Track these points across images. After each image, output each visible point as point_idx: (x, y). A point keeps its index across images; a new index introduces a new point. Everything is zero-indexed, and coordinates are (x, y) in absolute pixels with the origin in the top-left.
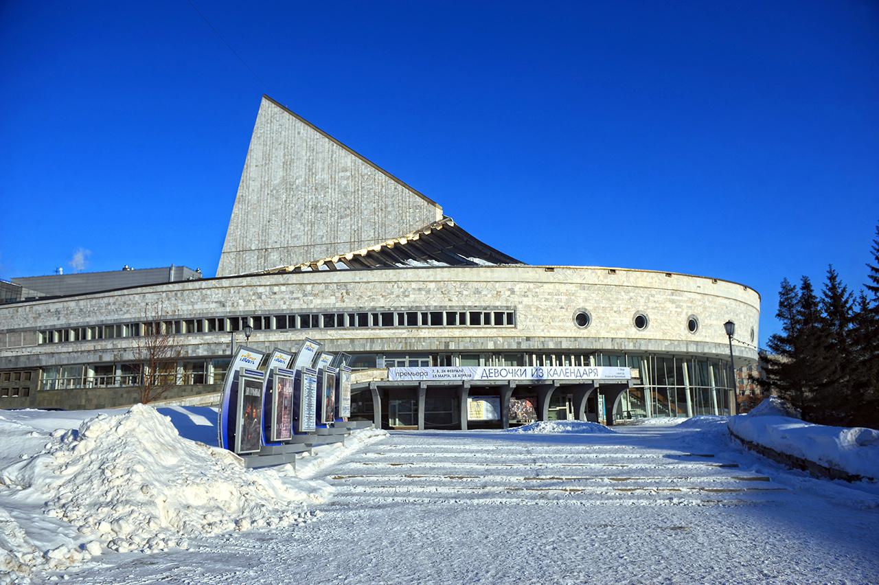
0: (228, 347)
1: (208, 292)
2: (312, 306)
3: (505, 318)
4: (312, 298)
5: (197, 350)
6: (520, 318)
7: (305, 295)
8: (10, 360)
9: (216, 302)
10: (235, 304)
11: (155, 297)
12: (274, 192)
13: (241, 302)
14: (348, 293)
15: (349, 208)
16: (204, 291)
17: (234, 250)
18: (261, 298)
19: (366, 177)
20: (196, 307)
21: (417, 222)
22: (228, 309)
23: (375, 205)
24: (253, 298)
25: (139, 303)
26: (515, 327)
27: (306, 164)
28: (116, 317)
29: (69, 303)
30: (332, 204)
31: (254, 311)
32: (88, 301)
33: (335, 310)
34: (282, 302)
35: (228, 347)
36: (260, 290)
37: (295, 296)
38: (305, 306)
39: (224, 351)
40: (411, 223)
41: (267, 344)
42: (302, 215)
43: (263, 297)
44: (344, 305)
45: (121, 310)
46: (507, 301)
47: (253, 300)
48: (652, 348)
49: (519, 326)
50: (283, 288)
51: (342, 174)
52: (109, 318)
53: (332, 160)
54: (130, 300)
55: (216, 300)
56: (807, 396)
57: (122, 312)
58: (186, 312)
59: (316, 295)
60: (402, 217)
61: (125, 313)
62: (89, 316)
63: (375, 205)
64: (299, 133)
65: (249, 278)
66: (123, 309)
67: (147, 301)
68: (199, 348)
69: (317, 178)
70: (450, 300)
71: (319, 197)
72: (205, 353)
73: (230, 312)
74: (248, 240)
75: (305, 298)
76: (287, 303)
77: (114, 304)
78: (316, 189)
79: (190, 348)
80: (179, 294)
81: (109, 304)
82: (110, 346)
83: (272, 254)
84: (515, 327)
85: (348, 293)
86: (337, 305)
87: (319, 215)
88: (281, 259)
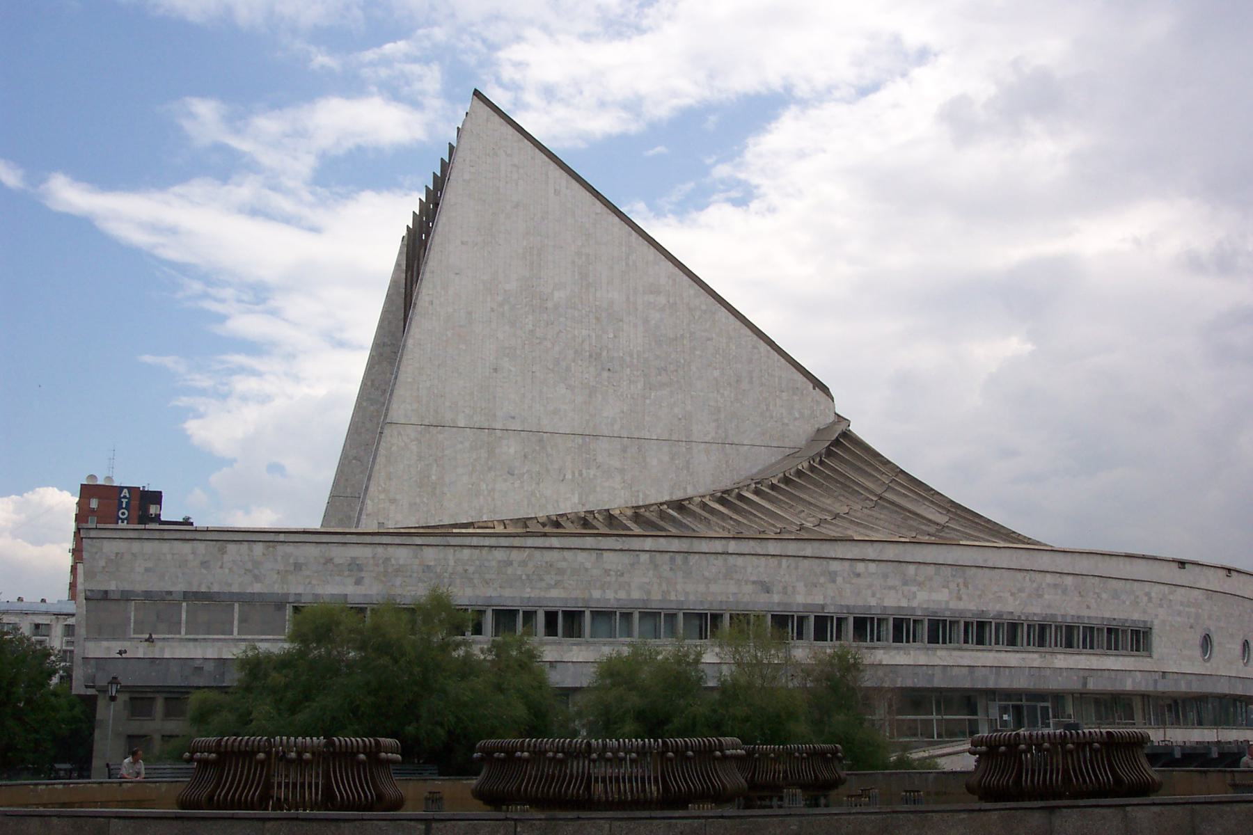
1: (740, 561)
2: (915, 604)
3: (1137, 638)
4: (914, 589)
6: (1159, 643)
7: (905, 583)
8: (201, 669)
9: (754, 582)
10: (790, 590)
11: (626, 559)
12: (506, 308)
13: (800, 586)
14: (966, 586)
15: (665, 370)
16: (731, 559)
17: (414, 420)
18: (834, 581)
19: (698, 313)
20: (714, 588)
21: (796, 419)
22: (776, 598)
24: (822, 580)
25: (586, 570)
26: (1150, 656)
27: (573, 262)
28: (528, 592)
29: (390, 549)
31: (823, 607)
32: (451, 550)
33: (948, 613)
34: (869, 592)
36: (835, 566)
37: (890, 582)
38: (904, 603)
40: (786, 421)
42: (568, 369)
43: (839, 580)
44: (961, 605)
45: (542, 580)
46: (1145, 612)
47: (822, 585)
48: (1004, 683)
49: (1155, 655)
51: (651, 298)
52: (508, 593)
53: (627, 264)
54: (565, 560)
57: (543, 584)
58: (692, 598)
59: (920, 584)
60: (768, 405)
61: (550, 587)
63: (716, 373)
64: (557, 192)
65: (816, 544)
67: (608, 567)
69: (598, 294)
70: (1088, 607)
71: (605, 336)
73: (779, 604)
74: (448, 404)
75: (906, 588)
76: (878, 596)
78: (598, 319)
80: (679, 558)
81: (510, 563)
84: (1150, 656)
85: (966, 586)
86: (952, 605)
87: (605, 374)
88: (525, 456)
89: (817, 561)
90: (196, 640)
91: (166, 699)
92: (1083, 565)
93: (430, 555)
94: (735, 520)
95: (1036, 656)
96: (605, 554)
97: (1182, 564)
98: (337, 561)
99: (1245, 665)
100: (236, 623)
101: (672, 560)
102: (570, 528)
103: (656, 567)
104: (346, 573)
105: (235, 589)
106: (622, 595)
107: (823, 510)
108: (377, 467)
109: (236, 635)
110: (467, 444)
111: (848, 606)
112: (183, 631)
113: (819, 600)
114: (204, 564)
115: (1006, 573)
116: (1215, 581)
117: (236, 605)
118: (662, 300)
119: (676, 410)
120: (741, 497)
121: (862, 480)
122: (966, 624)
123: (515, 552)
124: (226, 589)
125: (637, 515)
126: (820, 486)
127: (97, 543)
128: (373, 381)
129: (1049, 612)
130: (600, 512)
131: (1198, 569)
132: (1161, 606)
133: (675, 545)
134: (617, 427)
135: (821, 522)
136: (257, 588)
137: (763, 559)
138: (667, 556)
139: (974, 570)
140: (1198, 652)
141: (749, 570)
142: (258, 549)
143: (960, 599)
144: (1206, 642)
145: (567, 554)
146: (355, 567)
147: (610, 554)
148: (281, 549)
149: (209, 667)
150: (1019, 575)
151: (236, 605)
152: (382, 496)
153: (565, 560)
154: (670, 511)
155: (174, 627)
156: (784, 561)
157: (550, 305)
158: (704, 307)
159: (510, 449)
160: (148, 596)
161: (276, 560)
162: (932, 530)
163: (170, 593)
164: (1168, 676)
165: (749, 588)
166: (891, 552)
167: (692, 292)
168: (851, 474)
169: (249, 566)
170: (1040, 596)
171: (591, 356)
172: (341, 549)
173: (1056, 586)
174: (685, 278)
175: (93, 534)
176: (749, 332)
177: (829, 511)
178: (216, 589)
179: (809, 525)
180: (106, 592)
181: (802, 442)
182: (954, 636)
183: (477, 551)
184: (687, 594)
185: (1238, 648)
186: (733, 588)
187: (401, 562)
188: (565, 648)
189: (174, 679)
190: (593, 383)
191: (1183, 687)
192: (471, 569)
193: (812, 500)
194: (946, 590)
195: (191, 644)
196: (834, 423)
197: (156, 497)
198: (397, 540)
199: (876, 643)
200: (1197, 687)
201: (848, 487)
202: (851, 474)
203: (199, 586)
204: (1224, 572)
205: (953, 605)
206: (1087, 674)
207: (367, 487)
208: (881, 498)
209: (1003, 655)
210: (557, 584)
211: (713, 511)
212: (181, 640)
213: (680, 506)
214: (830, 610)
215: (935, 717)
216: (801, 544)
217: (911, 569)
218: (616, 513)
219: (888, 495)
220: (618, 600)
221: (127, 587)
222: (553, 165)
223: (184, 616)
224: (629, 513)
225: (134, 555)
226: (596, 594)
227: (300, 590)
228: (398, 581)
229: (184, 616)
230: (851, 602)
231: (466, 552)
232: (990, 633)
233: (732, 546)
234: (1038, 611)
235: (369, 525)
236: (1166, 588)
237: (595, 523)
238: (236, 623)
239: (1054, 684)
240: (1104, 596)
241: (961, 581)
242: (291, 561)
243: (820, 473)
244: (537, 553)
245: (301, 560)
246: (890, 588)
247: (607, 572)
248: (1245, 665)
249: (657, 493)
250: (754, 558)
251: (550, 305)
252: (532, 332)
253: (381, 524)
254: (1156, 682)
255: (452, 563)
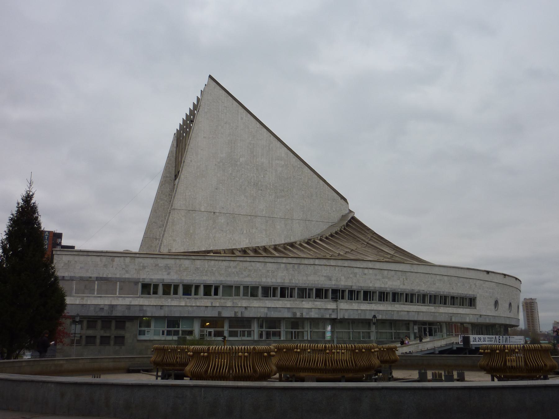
0: (333, 312)
1: (320, 267)
2: (387, 286)
3: (471, 302)
4: (387, 280)
5: (310, 313)
6: (479, 303)
7: (383, 278)
9: (325, 276)
11: (275, 266)
13: (343, 278)
14: (407, 279)
16: (316, 266)
22: (333, 283)
23: (303, 192)
26: (476, 308)
28: (236, 279)
29: (182, 261)
30: (270, 185)
31: (351, 286)
32: (207, 261)
33: (399, 290)
35: (333, 312)
36: (356, 270)
38: (383, 286)
39: (330, 315)
41: (359, 312)
42: (245, 189)
43: (358, 276)
44: (404, 287)
45: (242, 274)
47: (351, 278)
49: (477, 308)
50: (371, 271)
52: (229, 279)
53: (269, 148)
54: (251, 266)
55: (325, 274)
56: (457, 335)
58: (301, 282)
62: (206, 275)
64: (242, 118)
66: (244, 273)
68: (311, 312)
69: (257, 160)
72: (316, 316)
73: (334, 285)
77: (235, 267)
78: (257, 170)
79: (305, 311)
80: (296, 266)
82: (229, 304)
83: (220, 218)
84: (476, 308)
85: (407, 279)
87: (260, 192)
89: (349, 268)
90: (101, 297)
91: (88, 321)
92: (452, 272)
93: (198, 263)
94: (314, 251)
95: (433, 308)
96: (268, 264)
97: (488, 272)
98: (160, 265)
99: (510, 312)
100: (118, 290)
101: (293, 267)
102: (238, 254)
103: (287, 270)
104: (164, 270)
105: (118, 276)
106: (274, 280)
107: (347, 248)
108: (168, 227)
109: (96, 294)
110: (205, 218)
111: (361, 287)
112: (96, 293)
113: (350, 284)
114: (105, 266)
115: (422, 275)
116: (500, 280)
117: (118, 283)
118: (283, 163)
119: (287, 207)
120: (315, 242)
121: (360, 236)
122: (406, 294)
123: (232, 263)
124: (114, 276)
125: (276, 248)
126: (345, 238)
127: (60, 256)
128: (162, 191)
129: (438, 290)
130: (261, 247)
131: (493, 274)
132: (480, 289)
133: (295, 261)
134: (264, 213)
135: (346, 252)
136: (127, 276)
137: (329, 267)
138: (292, 265)
139: (410, 273)
140: (493, 307)
141: (323, 271)
142: (128, 260)
143: (404, 285)
144: (496, 303)
145: (253, 263)
146: (167, 268)
147: (270, 264)
148: (138, 260)
149: (106, 308)
150: (427, 276)
151: (118, 283)
152: (170, 238)
153: (251, 266)
154: (288, 247)
155: (92, 291)
156: (337, 268)
157: (238, 163)
158: (299, 166)
159: (222, 220)
160: (82, 279)
161: (135, 265)
162: (389, 256)
163: (91, 277)
164: (482, 317)
165: (323, 279)
166: (378, 265)
167: (294, 160)
168: (356, 234)
169: (124, 267)
170: (435, 284)
171: (254, 184)
172: (162, 261)
173: (440, 280)
174: (292, 154)
175: (58, 253)
176: (316, 177)
177: (349, 248)
178: (110, 276)
179: (341, 253)
180: (64, 277)
181: (336, 220)
182: (374, 298)
183: (217, 262)
184: (299, 280)
185: (508, 305)
186: (305, 278)
187: (187, 266)
188: (251, 301)
189: (91, 313)
190: (255, 195)
191: (488, 321)
192: (214, 269)
193: (342, 244)
194: (399, 281)
195: (99, 298)
196: (348, 213)
197: (60, 236)
198: (167, 257)
199: (372, 301)
200: (493, 321)
201: (356, 239)
202: (356, 234)
203: (103, 274)
204: (503, 276)
205: (402, 287)
206: (452, 315)
207: (163, 235)
208: (368, 243)
209: (420, 307)
210: (248, 276)
211: (304, 247)
212: (95, 297)
213: (292, 245)
214: (354, 288)
215: (393, 331)
216: (343, 261)
217: (386, 272)
218: (268, 247)
219: (370, 242)
220: (272, 282)
221: (72, 274)
222: (240, 107)
223: (96, 287)
224: (273, 247)
225: (76, 261)
226: (264, 280)
227: (144, 277)
228: (185, 274)
229: (96, 287)
230: (362, 285)
231: (213, 262)
232: (415, 299)
233: (317, 262)
234: (433, 290)
235: (164, 250)
236: (482, 282)
237: (260, 251)
238: (118, 290)
239: (439, 319)
240: (459, 284)
241: (404, 277)
242: (141, 265)
243: (344, 233)
244: (241, 263)
245: (146, 265)
246: (378, 280)
247: (268, 271)
248: (510, 312)
249: (281, 240)
250: (325, 267)
251: (238, 163)
252: (231, 174)
253: (170, 250)
254: (477, 319)
255: (207, 266)
